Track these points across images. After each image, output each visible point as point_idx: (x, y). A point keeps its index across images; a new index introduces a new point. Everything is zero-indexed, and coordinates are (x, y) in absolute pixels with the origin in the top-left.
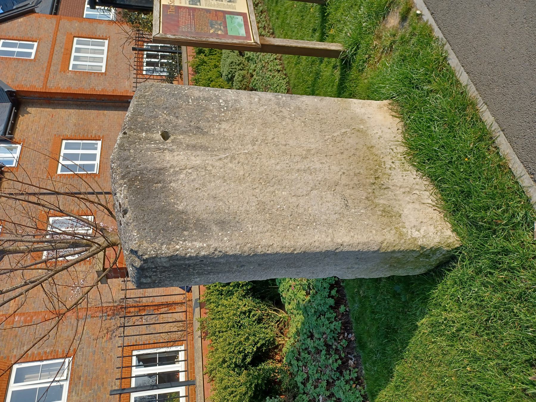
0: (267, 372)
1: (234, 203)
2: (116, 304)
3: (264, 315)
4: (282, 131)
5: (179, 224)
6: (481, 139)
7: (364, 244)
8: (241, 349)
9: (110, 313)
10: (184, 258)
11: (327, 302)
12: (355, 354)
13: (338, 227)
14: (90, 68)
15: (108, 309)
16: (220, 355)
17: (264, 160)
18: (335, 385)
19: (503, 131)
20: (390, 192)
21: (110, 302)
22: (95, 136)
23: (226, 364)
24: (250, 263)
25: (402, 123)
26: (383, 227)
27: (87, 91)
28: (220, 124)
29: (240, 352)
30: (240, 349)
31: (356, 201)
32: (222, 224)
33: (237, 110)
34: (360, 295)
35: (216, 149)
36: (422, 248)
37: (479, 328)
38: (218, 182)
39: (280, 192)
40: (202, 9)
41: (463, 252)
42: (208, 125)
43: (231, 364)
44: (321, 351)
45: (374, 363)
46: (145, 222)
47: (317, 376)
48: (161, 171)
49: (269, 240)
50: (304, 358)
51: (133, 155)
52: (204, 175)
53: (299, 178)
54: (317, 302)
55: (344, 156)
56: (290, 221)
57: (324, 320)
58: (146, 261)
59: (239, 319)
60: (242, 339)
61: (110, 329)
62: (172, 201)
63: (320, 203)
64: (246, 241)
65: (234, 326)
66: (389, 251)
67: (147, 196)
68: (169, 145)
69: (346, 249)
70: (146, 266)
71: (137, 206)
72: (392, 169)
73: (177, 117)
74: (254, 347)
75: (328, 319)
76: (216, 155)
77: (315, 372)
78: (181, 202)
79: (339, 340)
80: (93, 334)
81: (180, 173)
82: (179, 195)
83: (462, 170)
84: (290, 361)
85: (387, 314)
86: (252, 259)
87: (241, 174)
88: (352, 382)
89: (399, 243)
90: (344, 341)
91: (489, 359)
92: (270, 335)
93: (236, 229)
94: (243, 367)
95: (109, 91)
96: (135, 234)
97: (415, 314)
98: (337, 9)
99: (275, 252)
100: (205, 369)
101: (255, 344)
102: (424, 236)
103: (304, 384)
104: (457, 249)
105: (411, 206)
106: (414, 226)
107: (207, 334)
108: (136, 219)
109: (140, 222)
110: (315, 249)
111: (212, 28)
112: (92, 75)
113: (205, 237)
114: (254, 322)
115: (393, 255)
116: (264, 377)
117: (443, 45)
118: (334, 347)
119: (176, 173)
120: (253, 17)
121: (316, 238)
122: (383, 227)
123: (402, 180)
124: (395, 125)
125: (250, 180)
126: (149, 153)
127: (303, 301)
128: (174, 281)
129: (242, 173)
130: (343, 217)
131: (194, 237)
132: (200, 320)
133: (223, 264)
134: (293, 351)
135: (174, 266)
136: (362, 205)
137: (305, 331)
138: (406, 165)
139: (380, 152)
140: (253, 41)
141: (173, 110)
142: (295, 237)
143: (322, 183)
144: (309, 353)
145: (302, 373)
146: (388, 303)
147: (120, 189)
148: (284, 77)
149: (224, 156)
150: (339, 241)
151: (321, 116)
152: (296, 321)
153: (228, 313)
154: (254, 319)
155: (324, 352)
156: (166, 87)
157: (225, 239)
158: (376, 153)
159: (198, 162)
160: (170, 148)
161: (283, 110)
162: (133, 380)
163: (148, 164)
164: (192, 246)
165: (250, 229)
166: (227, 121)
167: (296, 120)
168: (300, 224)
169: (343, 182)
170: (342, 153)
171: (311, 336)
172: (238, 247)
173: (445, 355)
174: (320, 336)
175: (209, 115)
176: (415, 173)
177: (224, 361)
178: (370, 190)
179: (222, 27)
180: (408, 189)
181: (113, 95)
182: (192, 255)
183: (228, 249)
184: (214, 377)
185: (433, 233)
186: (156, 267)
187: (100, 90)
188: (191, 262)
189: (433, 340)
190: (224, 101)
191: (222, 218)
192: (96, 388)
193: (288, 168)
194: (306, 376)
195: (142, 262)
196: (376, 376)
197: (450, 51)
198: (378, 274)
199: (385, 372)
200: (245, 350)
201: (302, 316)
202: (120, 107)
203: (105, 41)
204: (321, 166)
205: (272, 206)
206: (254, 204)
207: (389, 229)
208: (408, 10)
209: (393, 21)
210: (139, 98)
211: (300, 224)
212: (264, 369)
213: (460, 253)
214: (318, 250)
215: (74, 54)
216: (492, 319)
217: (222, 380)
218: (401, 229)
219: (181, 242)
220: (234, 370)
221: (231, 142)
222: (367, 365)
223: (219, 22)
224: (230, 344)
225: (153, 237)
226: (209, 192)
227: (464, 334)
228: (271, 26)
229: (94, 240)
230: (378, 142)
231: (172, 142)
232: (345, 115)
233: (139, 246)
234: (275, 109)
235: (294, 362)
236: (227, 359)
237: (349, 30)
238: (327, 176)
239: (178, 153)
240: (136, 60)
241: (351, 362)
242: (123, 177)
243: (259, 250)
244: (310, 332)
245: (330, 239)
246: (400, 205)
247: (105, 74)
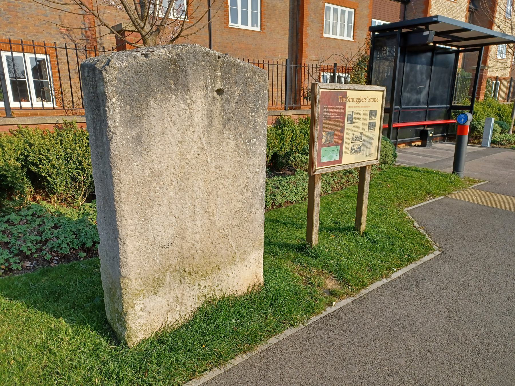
0: (21, 187)
1: (159, 150)
2: (98, 39)
3: (79, 183)
4: (230, 192)
5: (136, 101)
6: (220, 356)
7: (126, 263)
8: (43, 161)
9: (89, 33)
10: (104, 106)
11: (89, 240)
12: (37, 267)
13: (142, 240)
14: (328, 23)
15: (92, 32)
16: (37, 141)
17: (202, 176)
18: (4, 249)
19: (225, 372)
20: (177, 285)
21: (100, 33)
23: (28, 147)
24: (104, 164)
25: (242, 294)
26: (143, 279)
27: (306, 20)
28: (233, 139)
29: (40, 160)
30: (44, 160)
31: (167, 255)
32: (139, 139)
33: (247, 153)
34: (94, 269)
35: (209, 135)
36: (126, 314)
37: (50, 368)
38: (179, 136)
39: (172, 189)
40: (344, 126)
41: (123, 350)
42: (232, 128)
43: (28, 151)
44: (41, 236)
45: (26, 284)
46: (136, 72)
47: (15, 233)
48: (186, 87)
49: (127, 179)
50: (35, 221)
51: (200, 64)
52: (184, 125)
53: (187, 206)
54: (89, 232)
55: (209, 245)
56: (145, 199)
57: (71, 238)
58: (100, 72)
59: (74, 159)
60: (54, 162)
61: (71, 33)
62: (158, 97)
63: (164, 224)
64: (123, 160)
65: (67, 154)
66: (121, 285)
67: (162, 74)
68: (211, 95)
69: (121, 247)
70: (97, 72)
71: (152, 66)
72: (199, 286)
73: (237, 102)
74: (46, 173)
75: (72, 242)
76: (204, 135)
77: (19, 231)
78: (157, 104)
79: (51, 252)
81: (185, 104)
82: (164, 102)
83: (195, 343)
84: (32, 209)
85: (73, 292)
86: (107, 165)
87: (188, 156)
88: (7, 265)
89: (129, 293)
90: (50, 256)
91: (21, 377)
92: (59, 189)
93: (135, 151)
94: (26, 163)
95: (306, 40)
96: (124, 64)
97: (70, 315)
98: (350, 240)
99: (115, 185)
100: (24, 126)
101: (49, 175)
102: (136, 315)
103: (8, 221)
104: (126, 344)
105: (164, 303)
106: (145, 306)
107: (60, 128)
108: (139, 65)
109: (136, 69)
110: (119, 220)
111: (327, 134)
112: (320, 25)
113: (125, 124)
114: (72, 173)
115: (118, 289)
116: (15, 184)
117: (303, 324)
118: (44, 248)
119: (185, 100)
120: (337, 169)
121: (130, 221)
122: (143, 279)
123: (189, 295)
124: (241, 288)
125: (182, 163)
126: (202, 78)
127: (91, 219)
128: (87, 97)
129: (189, 157)
130: (151, 245)
131: (124, 114)
132: (74, 122)
133: (102, 140)
134: (41, 210)
135: (98, 97)
136: (164, 261)
137: (61, 221)
138: (204, 299)
139: (215, 276)
140: (316, 168)
141: (243, 98)
142: (129, 202)
143: (183, 226)
144: (39, 226)
145: (18, 219)
146: (83, 293)
147: (167, 52)
148: (303, 199)
149: (204, 142)
150: (128, 241)
151: (245, 225)
152: (71, 213)
153: (80, 148)
154: (75, 174)
155: (39, 238)
156: (264, 93)
157: (124, 142)
158: (214, 273)
159: (196, 119)
160: (208, 96)
161: (250, 193)
162: (21, 55)
163: (192, 77)
164: (116, 113)
165: (135, 164)
166: (237, 145)
167: (241, 204)
168: (143, 207)
169: (184, 245)
170: (212, 243)
171: (56, 227)
172: (117, 153)
173: (28, 342)
174: (55, 234)
175: (241, 130)
176: (196, 306)
177: (31, 145)
178: (178, 267)
179: (328, 142)
180: (180, 300)
181: (302, 44)
182: (108, 113)
183: (115, 144)
184: (15, 135)
185: (139, 323)
186: (96, 81)
187: (307, 32)
188: (102, 112)
189: (43, 331)
190: (255, 142)
191: (144, 139)
192: (7, 16)
193: (195, 197)
194: (16, 223)
195: (100, 70)
196: (12, 286)
197: (297, 329)
198: (104, 279)
199: (16, 294)
200: (43, 165)
201: (77, 218)
202: (293, 50)
203: (352, 38)
204: (199, 225)
205: (158, 183)
206: (159, 167)
207: (142, 284)
208: (337, 296)
209: (331, 284)
210: (252, 70)
211: (143, 207)
212: (24, 183)
213: (123, 348)
214: (118, 223)
215: (340, 8)
216: (58, 377)
217: (11, 143)
218: (142, 295)
219: (119, 103)
220: (22, 154)
221: (217, 148)
222: (24, 278)
223: (332, 140)
224: (49, 150)
225: (122, 79)
226: (169, 128)
227: (46, 355)
228: (348, 187)
229: (147, 23)
230: (224, 274)
231: (214, 98)
232: (248, 245)
233: (114, 68)
234: (250, 186)
235: (31, 212)
236: (32, 147)
237: (329, 249)
238: (189, 231)
239: (204, 103)
240: (326, 66)
241: (28, 264)
242: (178, 55)
243: (115, 171)
244: (60, 226)
245: (129, 233)
246: (165, 294)
247: (322, 37)
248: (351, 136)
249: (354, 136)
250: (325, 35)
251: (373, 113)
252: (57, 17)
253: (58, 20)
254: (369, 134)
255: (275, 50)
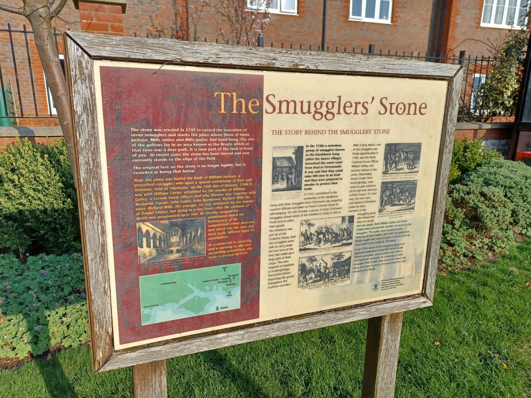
14: (489, 8)
15: (184, 32)
22: (396, 17)
80: (156, 16)
112: (477, 11)
248: (295, 229)
249: (313, 230)
250: (483, 25)
251: (401, 154)
252: (148, 18)
253: (149, 21)
254: (386, 219)
255: (408, 47)
